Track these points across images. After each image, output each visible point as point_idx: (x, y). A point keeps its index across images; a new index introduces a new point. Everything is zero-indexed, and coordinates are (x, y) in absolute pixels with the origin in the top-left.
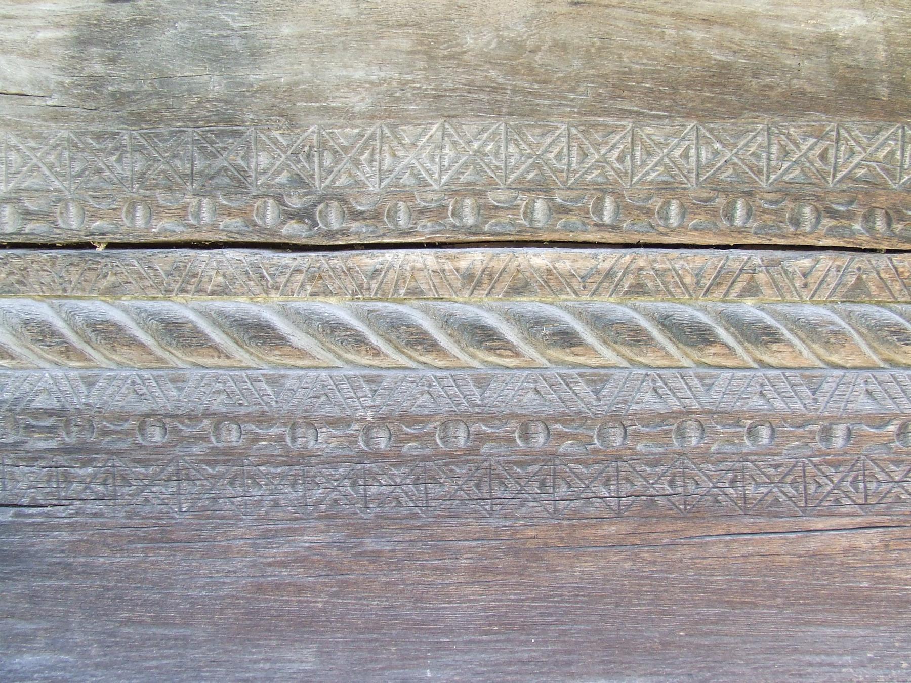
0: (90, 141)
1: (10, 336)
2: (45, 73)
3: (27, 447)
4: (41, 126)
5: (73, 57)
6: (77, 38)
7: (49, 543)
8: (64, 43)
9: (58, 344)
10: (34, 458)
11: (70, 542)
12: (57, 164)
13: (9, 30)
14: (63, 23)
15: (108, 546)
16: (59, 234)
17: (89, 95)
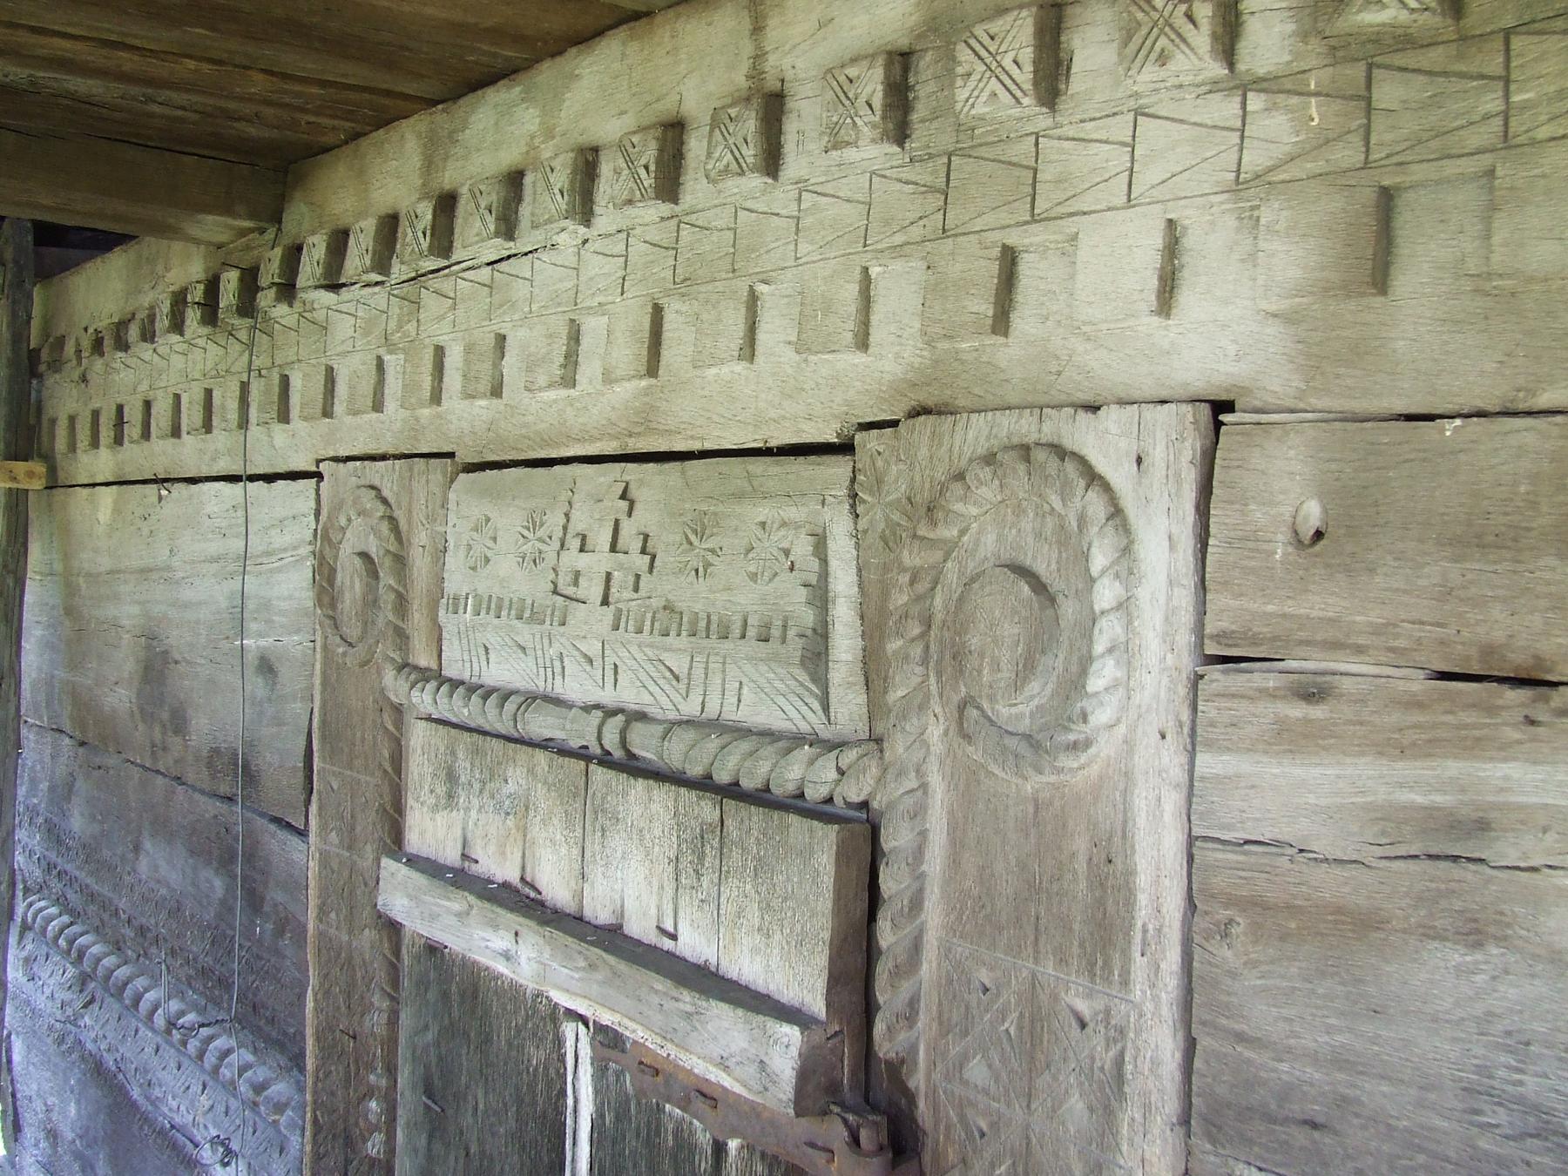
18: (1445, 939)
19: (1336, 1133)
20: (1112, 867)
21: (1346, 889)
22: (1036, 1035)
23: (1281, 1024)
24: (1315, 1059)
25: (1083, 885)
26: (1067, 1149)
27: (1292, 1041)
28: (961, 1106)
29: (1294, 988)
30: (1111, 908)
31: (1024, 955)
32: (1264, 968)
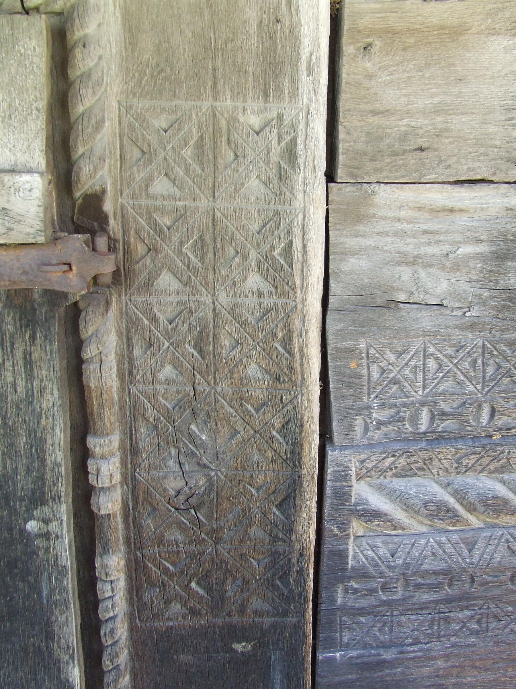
0: (505, 349)
1: (401, 511)
2: (465, 286)
3: (415, 600)
4: (458, 335)
5: (491, 271)
6: (494, 253)
7: (426, 671)
8: (483, 257)
9: (450, 518)
10: (423, 607)
11: (444, 668)
12: (471, 370)
13: (429, 244)
14: (482, 238)
15: (476, 668)
16: (470, 431)
17: (504, 307)
18: (499, 34)
19: (435, 150)
20: (279, 25)
21: (445, 15)
22: (213, 144)
23: (402, 99)
24: (424, 113)
25: (254, 40)
26: (352, 657)
27: (410, 107)
28: (148, 212)
29: (411, 77)
30: (280, 51)
31: (203, 97)
32: (392, 69)
